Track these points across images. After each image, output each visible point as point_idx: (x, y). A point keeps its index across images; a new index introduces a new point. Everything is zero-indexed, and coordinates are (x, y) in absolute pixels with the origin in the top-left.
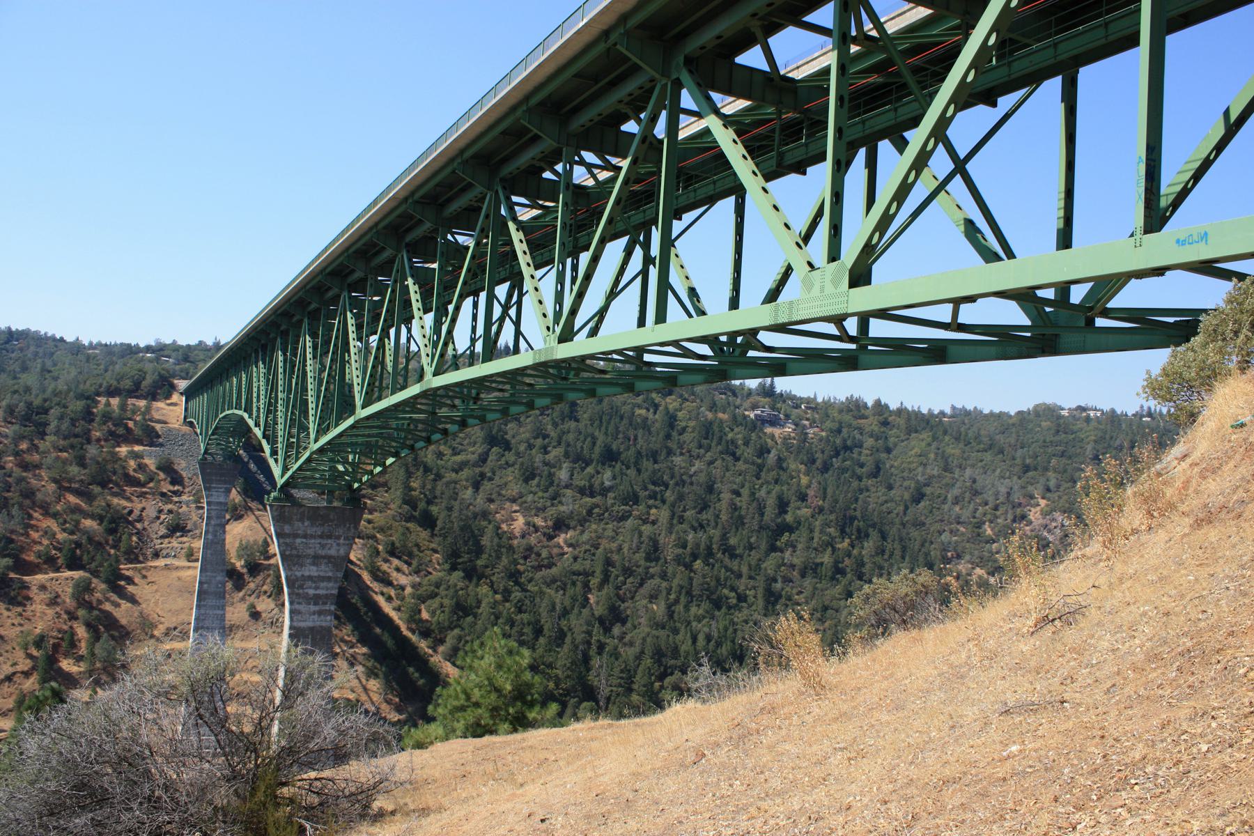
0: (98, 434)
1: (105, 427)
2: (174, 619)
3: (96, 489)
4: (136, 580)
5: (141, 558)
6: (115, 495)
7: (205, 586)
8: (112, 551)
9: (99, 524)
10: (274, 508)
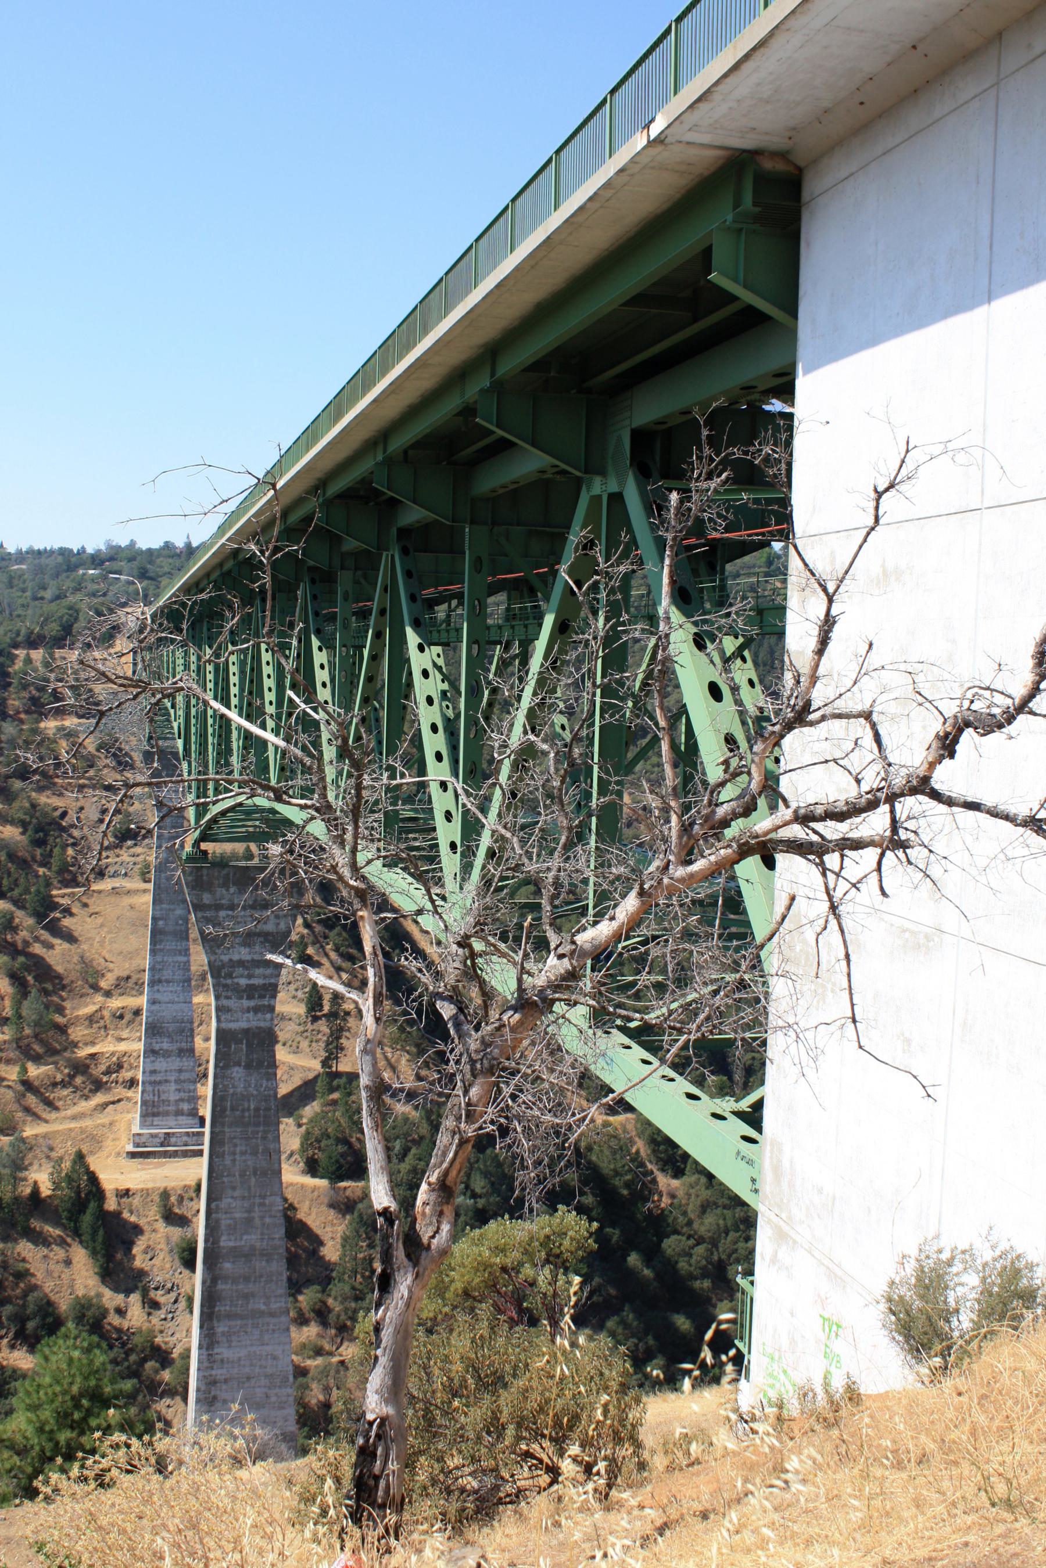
0: (17, 703)
2: (127, 965)
4: (74, 910)
6: (40, 789)
7: (161, 923)
8: (41, 871)
9: (23, 833)
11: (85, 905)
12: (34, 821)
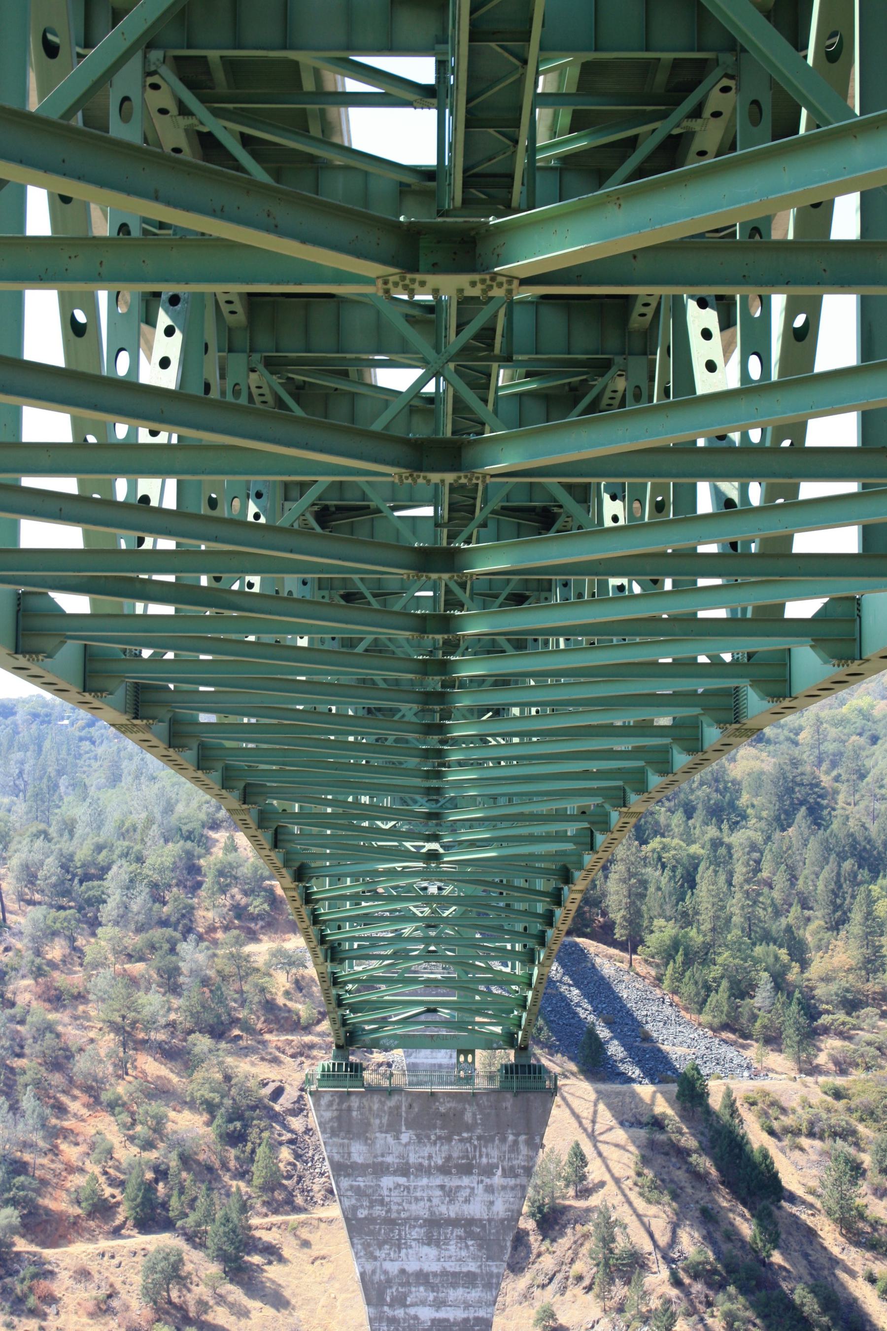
0: (210, 915)
1: (225, 901)
3: (202, 1043)
4: (286, 1253)
5: (299, 1200)
6: (245, 1052)
10: (324, 1101)
11: (306, 1244)
12: (228, 1102)
